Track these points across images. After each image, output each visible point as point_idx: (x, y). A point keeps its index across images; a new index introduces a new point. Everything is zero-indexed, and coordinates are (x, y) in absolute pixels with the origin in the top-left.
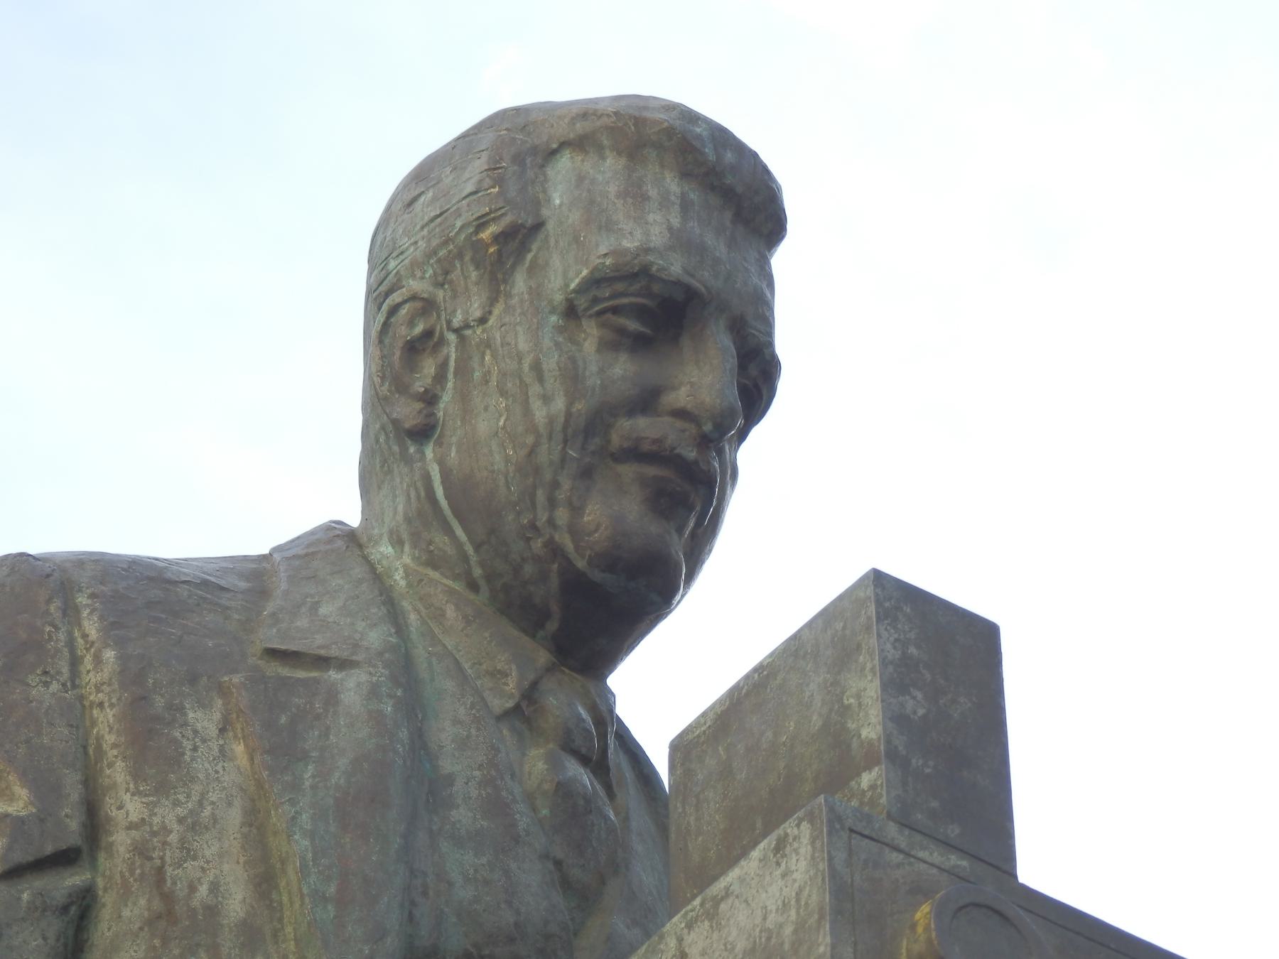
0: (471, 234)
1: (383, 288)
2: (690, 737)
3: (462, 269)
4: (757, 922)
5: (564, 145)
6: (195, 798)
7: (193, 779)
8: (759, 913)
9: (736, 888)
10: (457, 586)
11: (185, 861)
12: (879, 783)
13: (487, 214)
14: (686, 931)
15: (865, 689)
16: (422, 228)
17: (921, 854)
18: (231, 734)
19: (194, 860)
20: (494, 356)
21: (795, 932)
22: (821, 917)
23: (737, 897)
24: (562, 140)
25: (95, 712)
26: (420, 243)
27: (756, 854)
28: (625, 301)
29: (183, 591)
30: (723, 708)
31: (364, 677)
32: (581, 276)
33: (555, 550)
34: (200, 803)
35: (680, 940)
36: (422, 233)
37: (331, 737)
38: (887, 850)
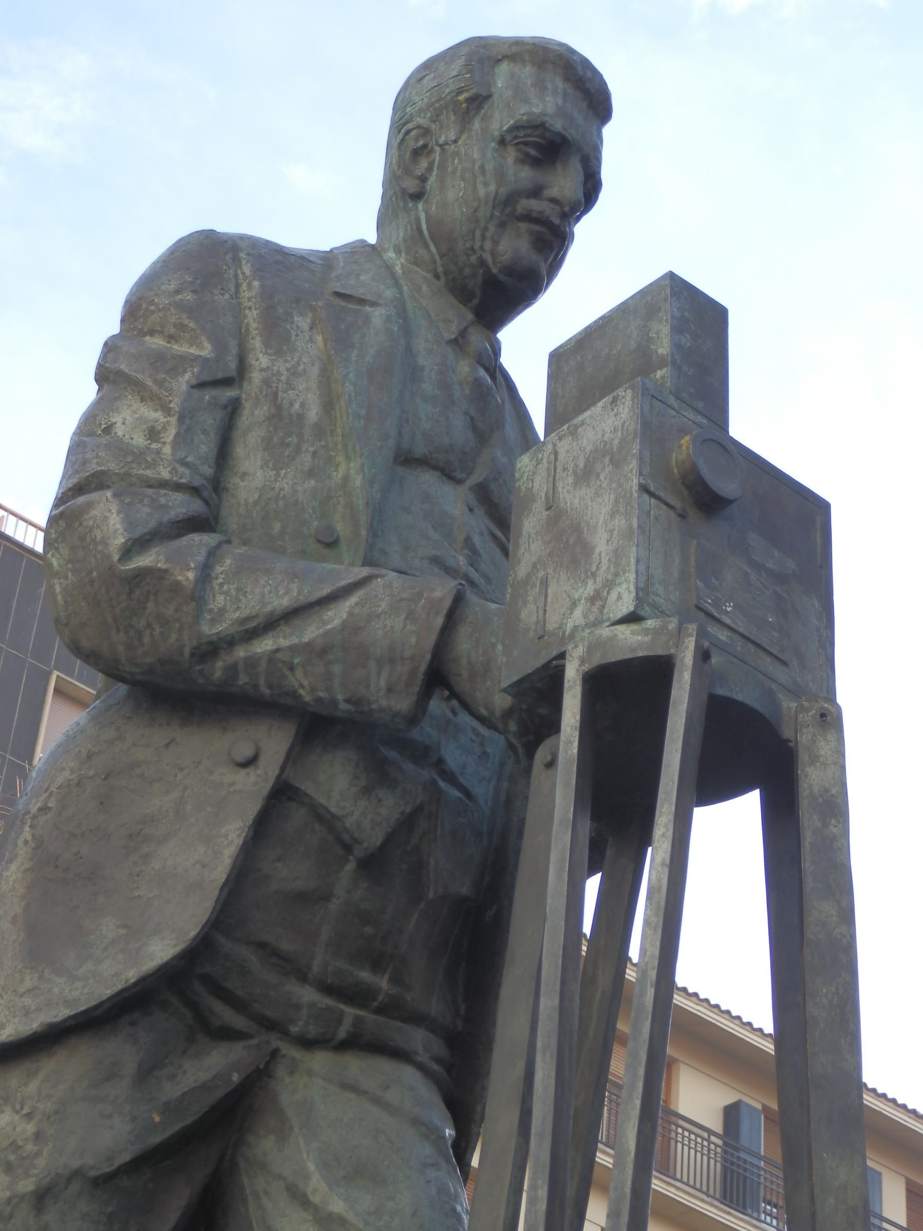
0: (454, 97)
1: (402, 121)
2: (561, 350)
3: (446, 114)
4: (598, 437)
5: (505, 57)
6: (296, 359)
7: (295, 350)
8: (600, 433)
9: (588, 421)
10: (428, 276)
11: (289, 390)
12: (666, 376)
13: (463, 87)
14: (558, 441)
15: (662, 330)
16: (427, 92)
17: (684, 413)
18: (315, 330)
19: (293, 390)
20: (460, 160)
21: (620, 443)
22: (635, 436)
23: (588, 425)
24: (504, 54)
25: (247, 311)
26: (425, 99)
27: (600, 404)
28: (531, 139)
29: (292, 259)
30: (581, 337)
31: (383, 312)
32: (509, 124)
33: (482, 263)
34: (298, 363)
35: (555, 445)
36: (426, 95)
37: (366, 338)
38: (669, 408)
